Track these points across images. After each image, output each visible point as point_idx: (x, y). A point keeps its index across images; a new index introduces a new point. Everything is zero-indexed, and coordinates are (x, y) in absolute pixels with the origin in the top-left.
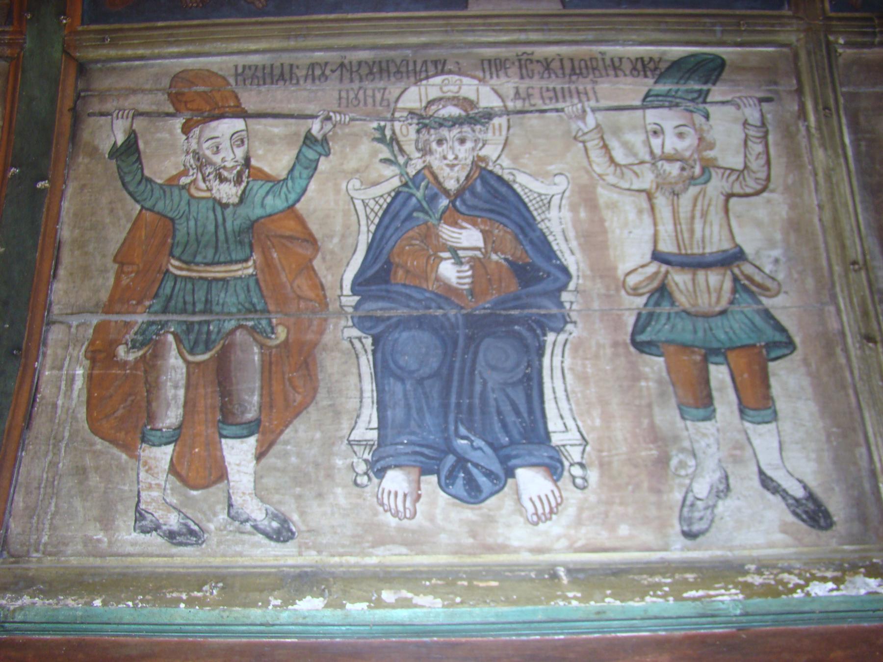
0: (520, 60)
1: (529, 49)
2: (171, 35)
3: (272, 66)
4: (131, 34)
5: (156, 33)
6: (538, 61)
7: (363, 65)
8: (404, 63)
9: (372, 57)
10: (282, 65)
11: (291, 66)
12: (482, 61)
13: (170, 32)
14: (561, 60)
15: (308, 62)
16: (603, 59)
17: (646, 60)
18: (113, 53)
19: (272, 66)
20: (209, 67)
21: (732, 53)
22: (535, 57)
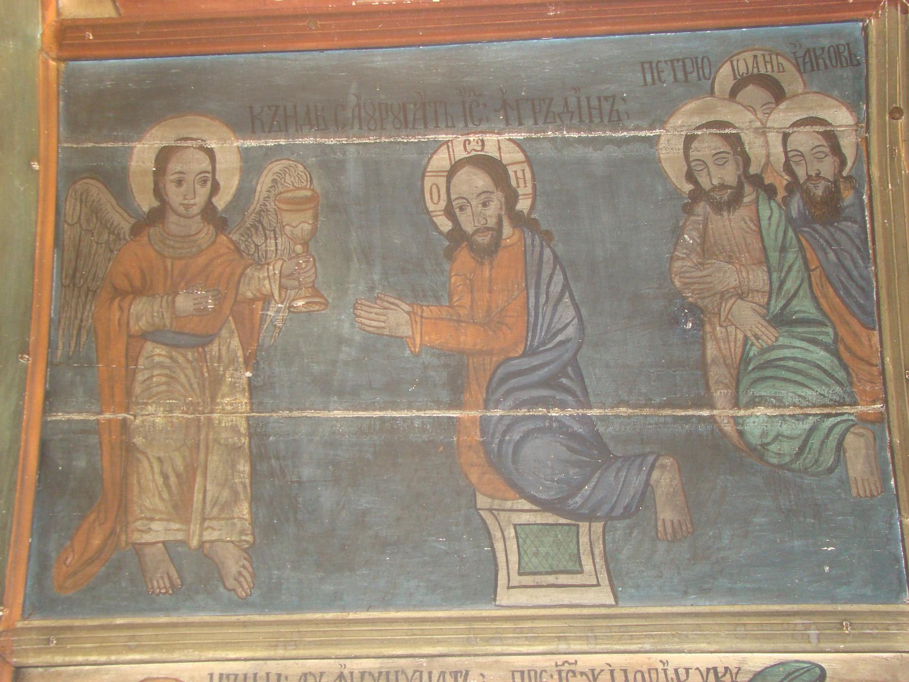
0: (560, 672)
1: (571, 658)
2: (132, 638)
3: (255, 675)
4: (83, 634)
5: (114, 634)
6: (582, 674)
7: (367, 675)
8: (417, 674)
9: (377, 666)
10: (268, 674)
11: (279, 675)
12: (513, 672)
13: (130, 633)
14: (612, 672)
15: (300, 671)
16: (665, 671)
17: (721, 670)
18: (59, 659)
19: (255, 675)
20: (177, 675)
21: (832, 660)
22: (579, 668)
